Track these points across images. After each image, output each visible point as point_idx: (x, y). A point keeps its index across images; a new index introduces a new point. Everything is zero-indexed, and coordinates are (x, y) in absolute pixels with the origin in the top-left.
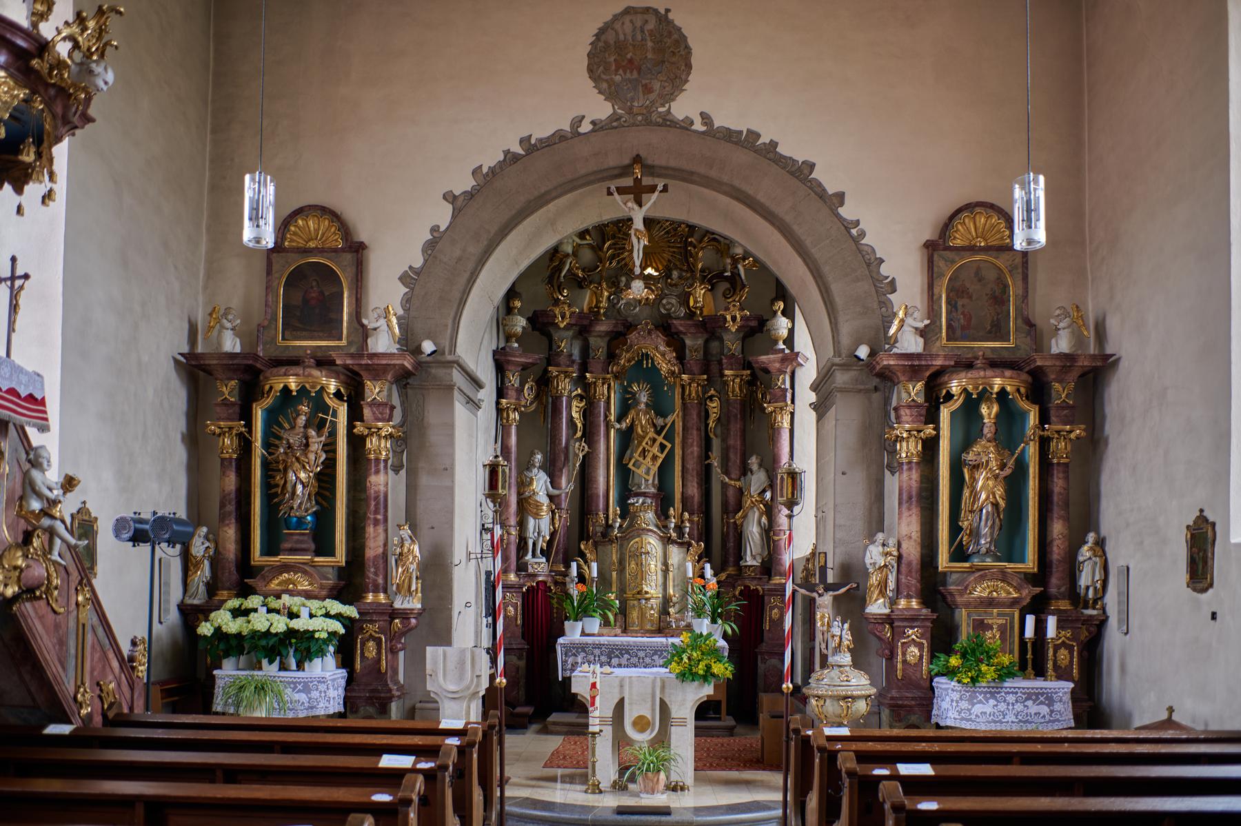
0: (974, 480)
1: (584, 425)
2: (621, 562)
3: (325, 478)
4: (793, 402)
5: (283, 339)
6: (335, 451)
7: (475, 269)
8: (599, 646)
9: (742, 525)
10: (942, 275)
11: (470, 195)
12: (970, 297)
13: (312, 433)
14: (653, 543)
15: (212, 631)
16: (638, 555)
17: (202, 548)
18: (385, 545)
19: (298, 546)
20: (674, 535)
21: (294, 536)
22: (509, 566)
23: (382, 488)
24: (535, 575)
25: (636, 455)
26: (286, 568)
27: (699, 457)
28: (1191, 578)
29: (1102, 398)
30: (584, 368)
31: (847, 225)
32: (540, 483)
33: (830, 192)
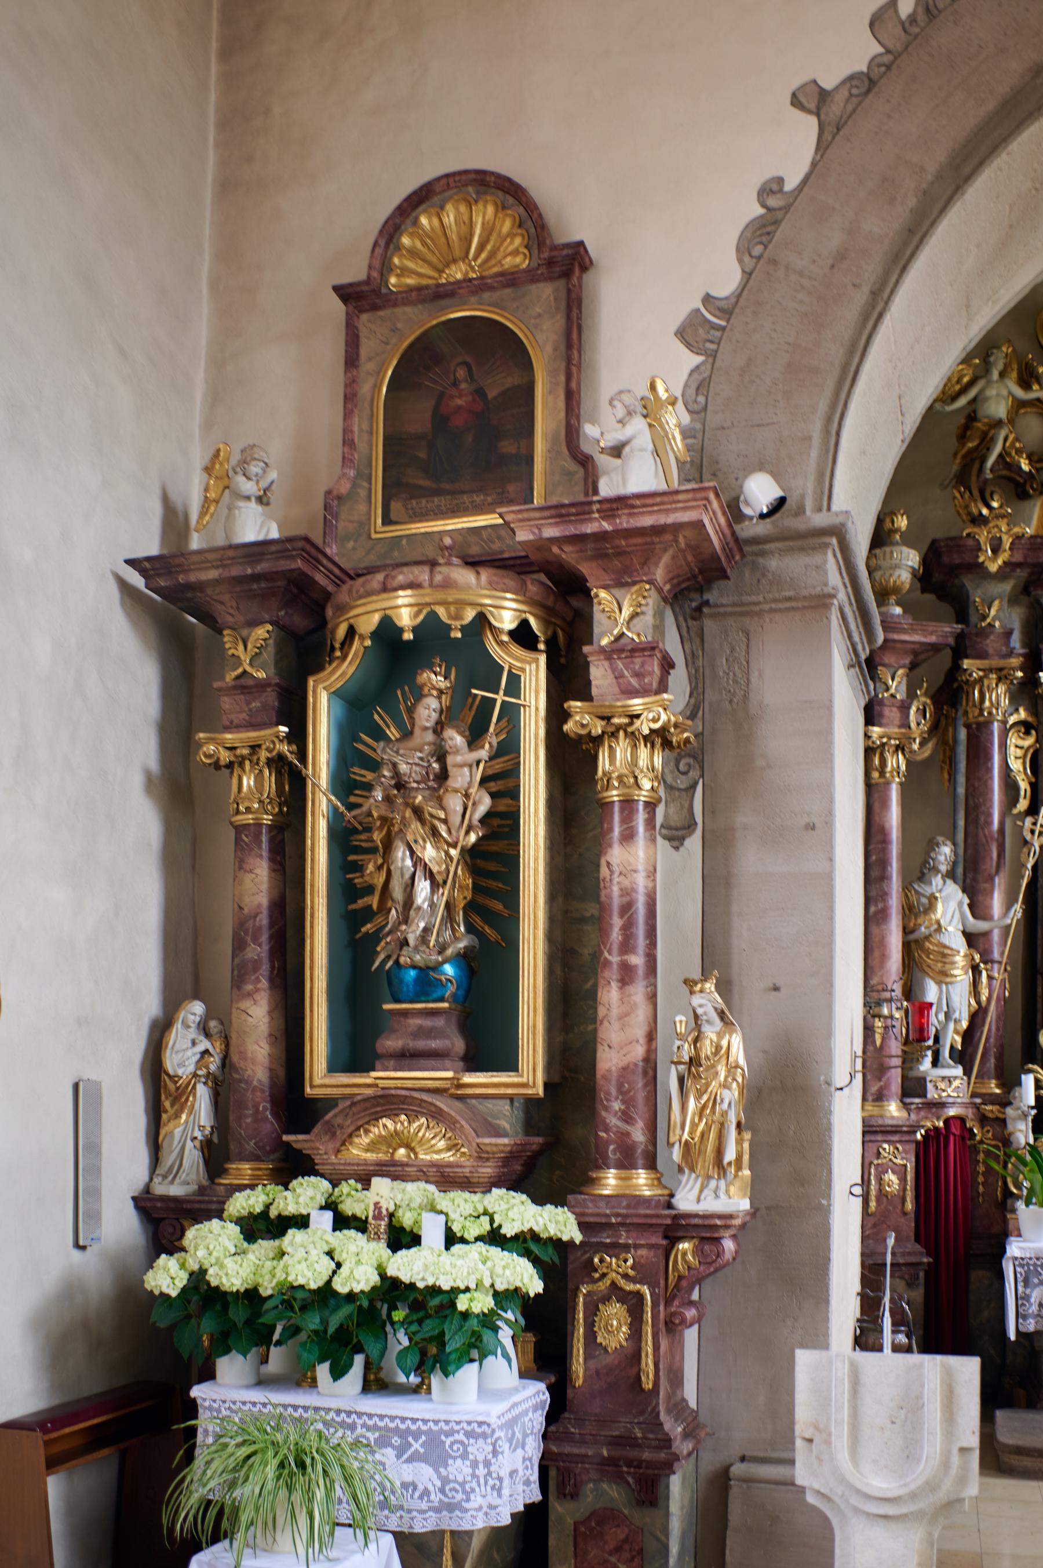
1: (1033, 786)
3: (492, 866)
5: (387, 521)
6: (514, 794)
7: (883, 281)
11: (865, 84)
13: (456, 739)
15: (182, 1279)
17: (192, 1057)
18: (651, 1037)
19: (422, 1044)
21: (414, 1018)
22: (887, 1086)
23: (641, 882)
24: (941, 1105)
26: (388, 1103)
32: (949, 908)
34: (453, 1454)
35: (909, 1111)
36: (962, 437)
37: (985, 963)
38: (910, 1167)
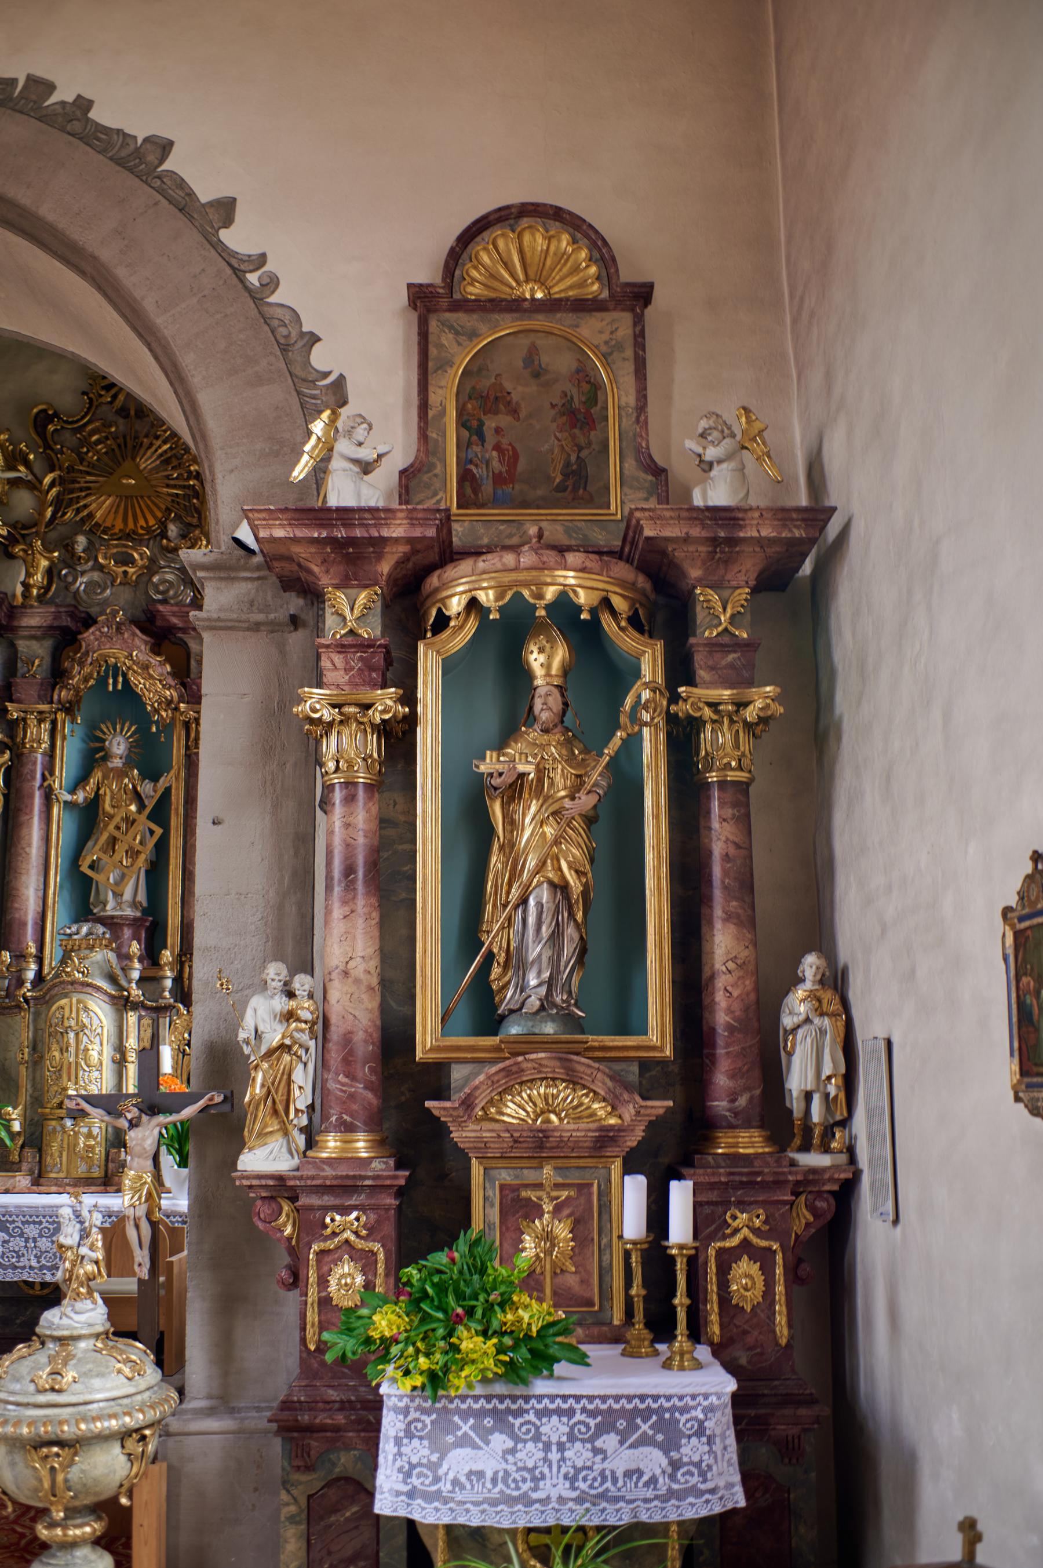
0: (511, 823)
10: (446, 364)
12: (514, 412)
28: (1024, 1072)
29: (827, 630)
31: (238, 266)
33: (203, 199)
34: (523, 1437)
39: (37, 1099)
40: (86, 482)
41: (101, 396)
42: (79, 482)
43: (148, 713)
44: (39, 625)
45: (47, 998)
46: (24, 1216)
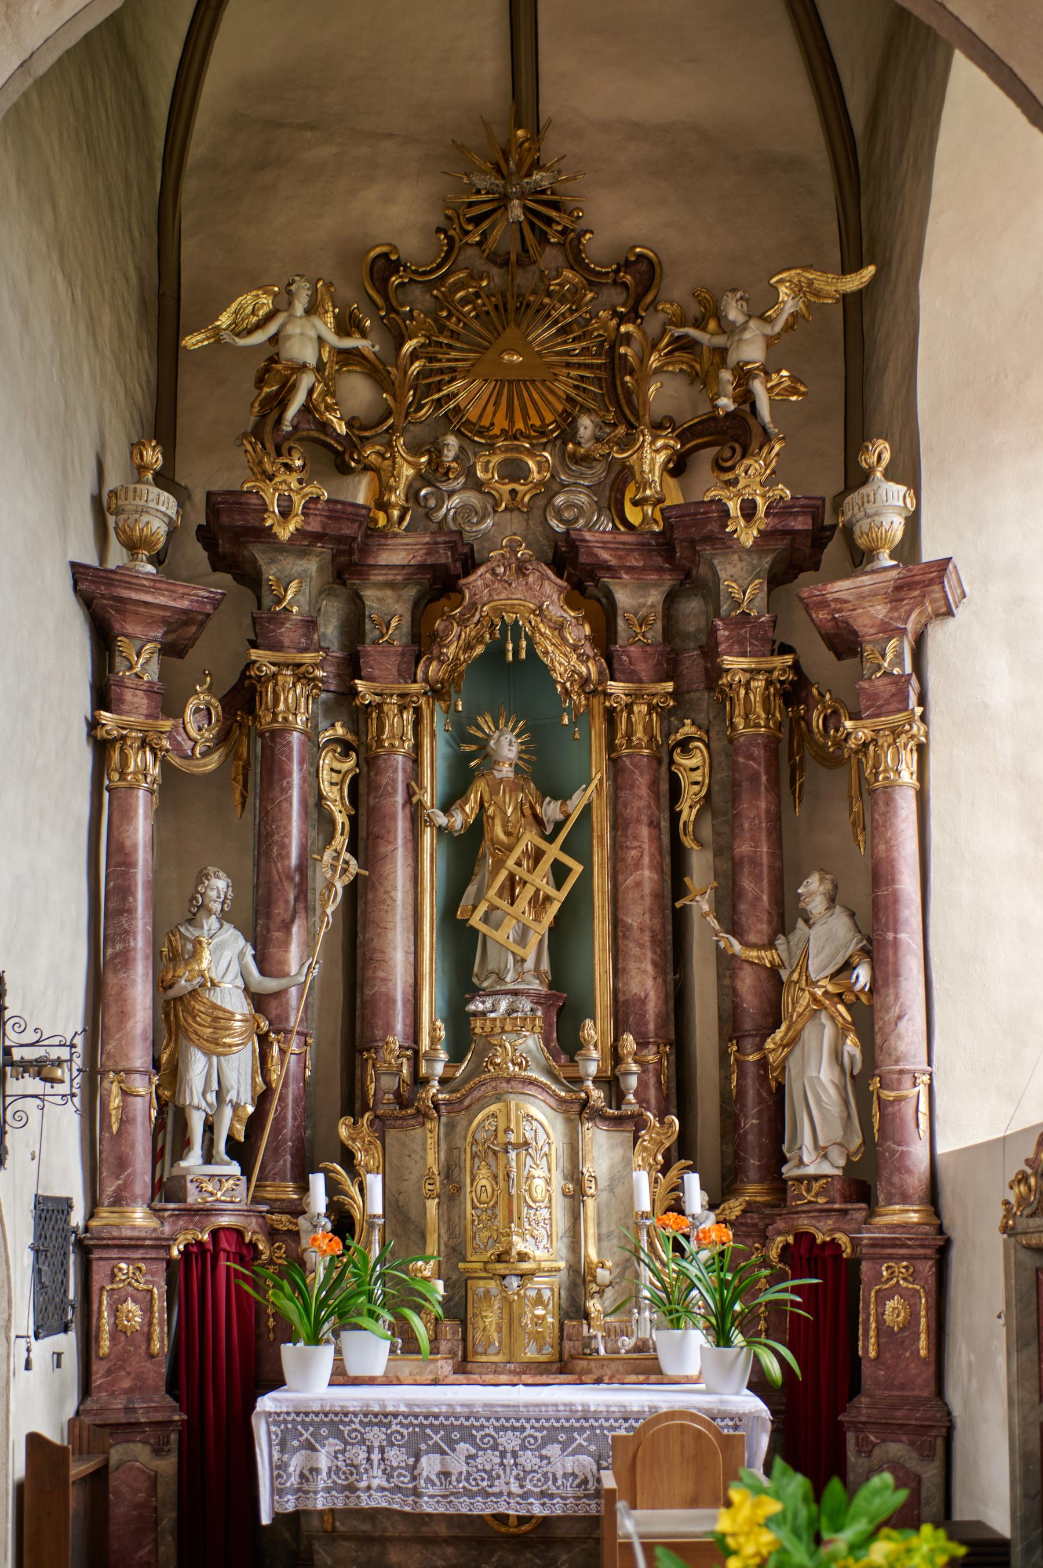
1: (353, 820)
2: (450, 1172)
4: (922, 701)
8: (382, 1418)
9: (783, 1068)
14: (539, 1118)
16: (498, 1149)
20: (597, 1095)
25: (492, 893)
27: (657, 896)
30: (352, 665)
32: (223, 959)
35: (162, 1220)
36: (260, 382)
37: (277, 1032)
38: (159, 1292)
39: (454, 1249)
40: (449, 360)
41: (467, 233)
42: (440, 361)
43: (559, 696)
44: (405, 562)
45: (467, 1102)
46: (498, 1419)
